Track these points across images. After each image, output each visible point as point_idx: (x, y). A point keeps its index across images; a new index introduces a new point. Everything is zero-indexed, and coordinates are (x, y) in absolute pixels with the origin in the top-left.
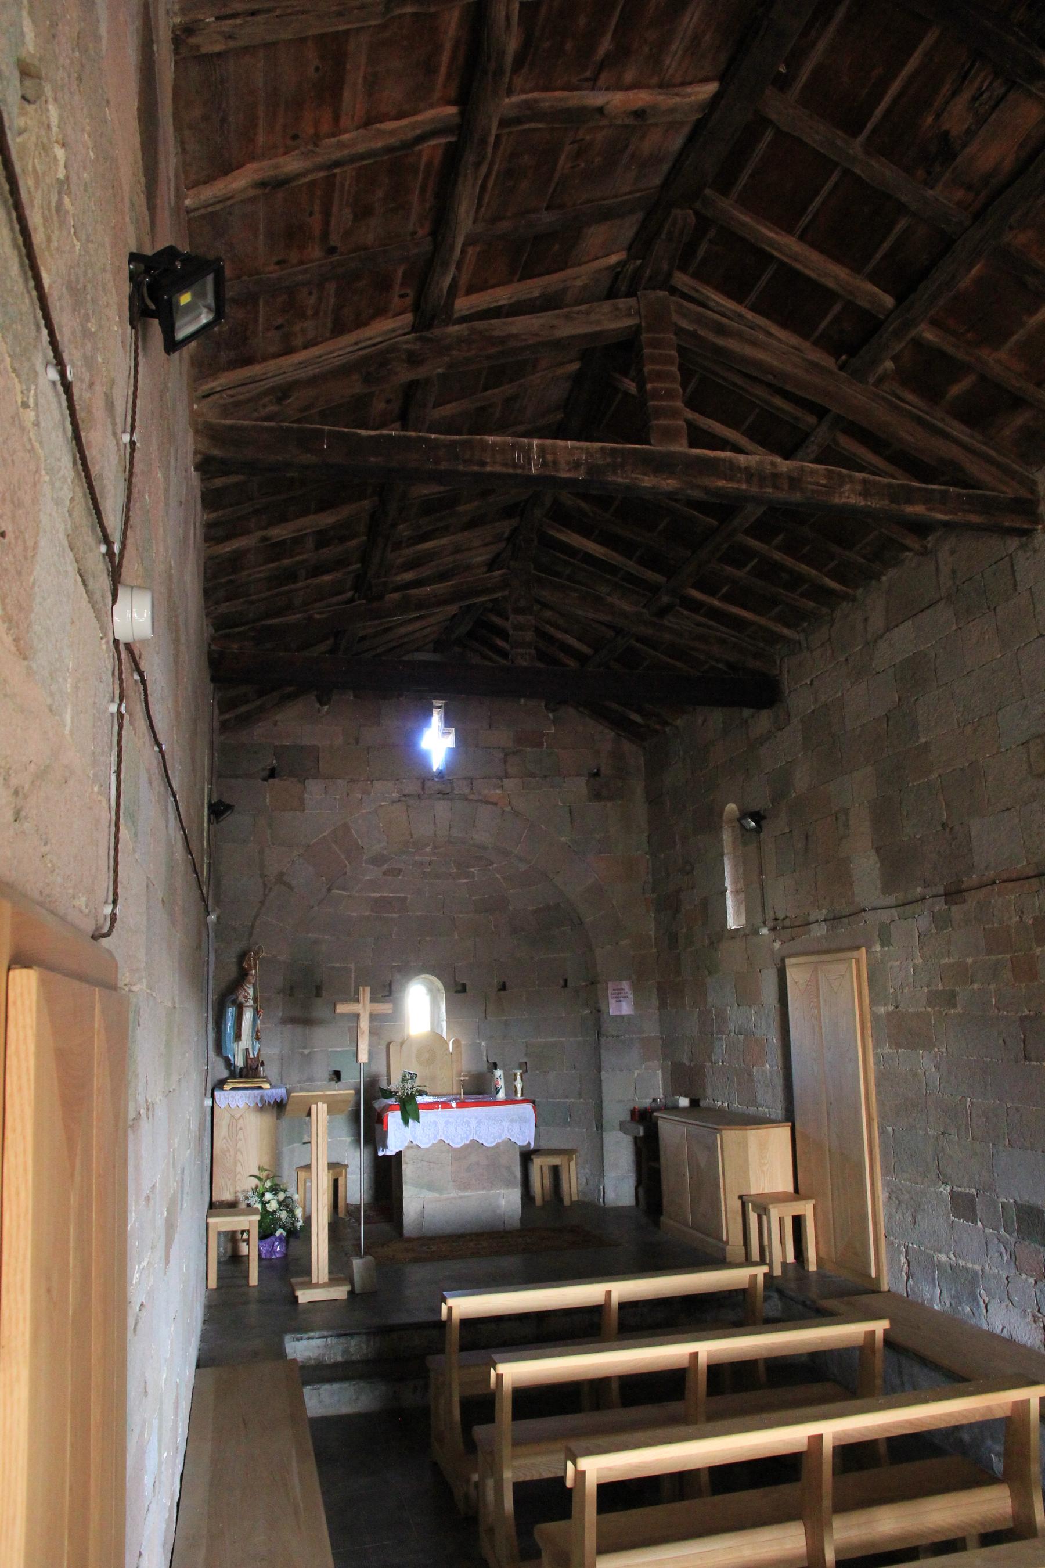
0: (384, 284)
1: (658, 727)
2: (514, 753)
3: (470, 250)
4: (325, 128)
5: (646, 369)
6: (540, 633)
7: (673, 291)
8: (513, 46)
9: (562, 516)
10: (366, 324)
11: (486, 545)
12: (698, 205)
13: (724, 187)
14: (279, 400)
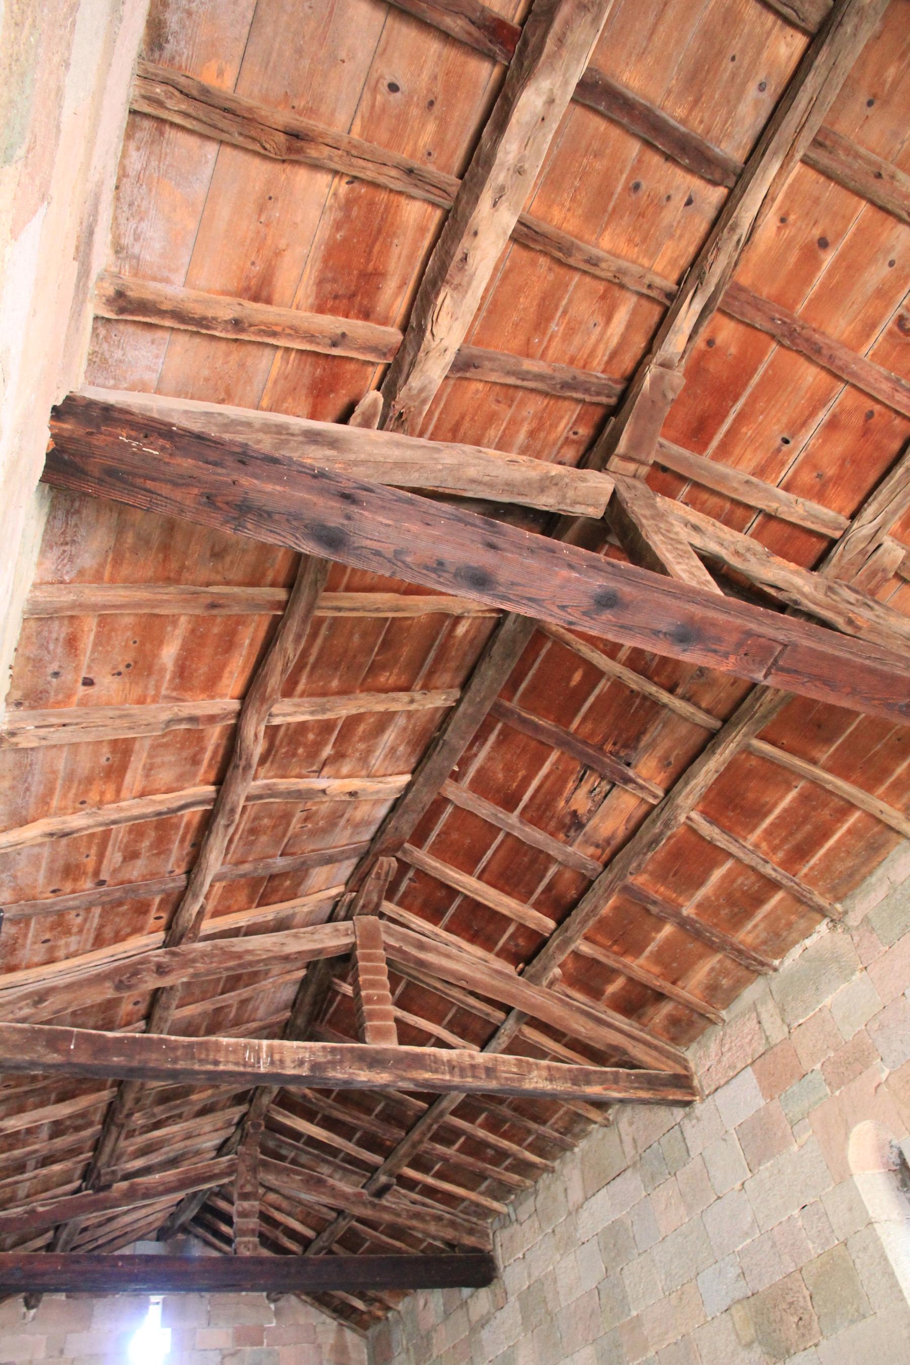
0: (142, 909)
1: (380, 1313)
2: (233, 1355)
3: (217, 885)
4: (109, 796)
5: (361, 979)
6: (265, 1217)
7: (382, 915)
8: (258, 750)
9: (285, 1101)
10: (123, 939)
11: (216, 1130)
12: (399, 854)
13: (419, 843)
14: (36, 1003)
